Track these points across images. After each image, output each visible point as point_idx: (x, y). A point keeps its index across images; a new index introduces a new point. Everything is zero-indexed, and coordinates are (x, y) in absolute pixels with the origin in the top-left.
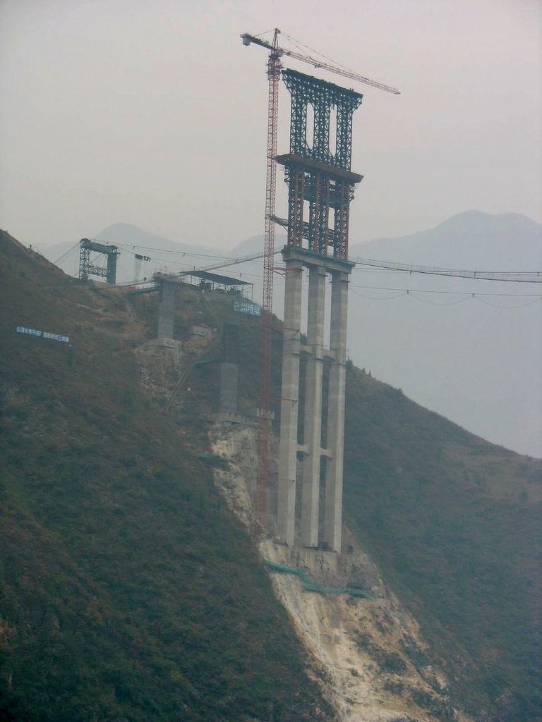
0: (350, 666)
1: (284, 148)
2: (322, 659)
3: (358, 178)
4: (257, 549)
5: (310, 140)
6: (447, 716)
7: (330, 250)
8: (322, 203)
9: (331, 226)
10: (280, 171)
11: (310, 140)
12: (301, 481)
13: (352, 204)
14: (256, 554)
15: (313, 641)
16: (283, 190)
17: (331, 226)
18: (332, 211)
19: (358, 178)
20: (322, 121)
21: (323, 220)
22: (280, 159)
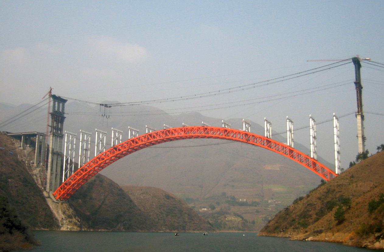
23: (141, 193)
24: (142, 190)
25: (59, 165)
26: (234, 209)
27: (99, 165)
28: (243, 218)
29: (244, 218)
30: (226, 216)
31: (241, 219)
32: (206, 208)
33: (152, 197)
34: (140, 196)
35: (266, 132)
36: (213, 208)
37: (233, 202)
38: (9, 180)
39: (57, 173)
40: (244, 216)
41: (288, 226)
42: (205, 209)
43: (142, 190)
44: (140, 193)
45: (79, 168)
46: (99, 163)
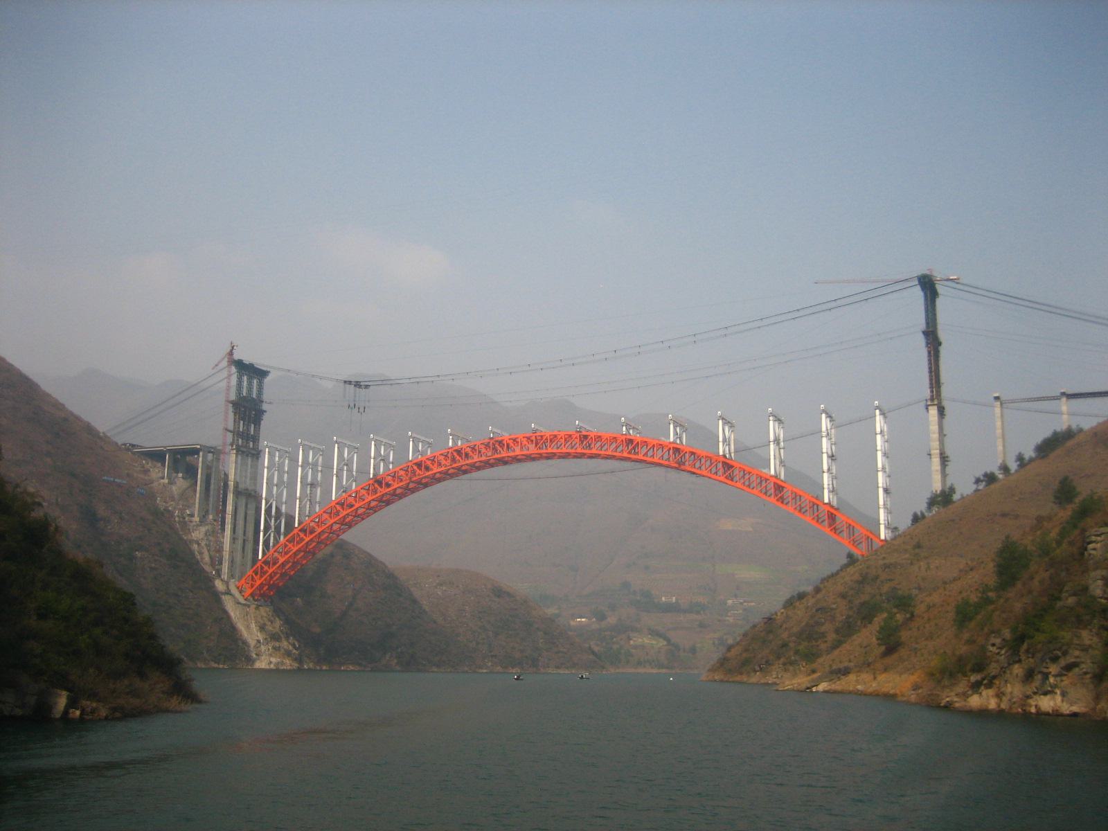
0: (257, 638)
1: (233, 397)
2: (217, 585)
3: (265, 411)
4: (214, 584)
5: (244, 393)
6: (492, 795)
7: (251, 445)
8: (247, 440)
9: (252, 433)
10: (231, 409)
11: (244, 393)
12: (231, 552)
13: (262, 422)
14: (214, 586)
15: (241, 626)
16: (231, 415)
17: (252, 433)
18: (253, 426)
19: (265, 411)
20: (250, 384)
21: (248, 430)
22: (232, 402)
24: (439, 576)
28: (668, 641)
31: (665, 643)
34: (436, 590)
36: (602, 617)
42: (583, 620)
44: (435, 584)
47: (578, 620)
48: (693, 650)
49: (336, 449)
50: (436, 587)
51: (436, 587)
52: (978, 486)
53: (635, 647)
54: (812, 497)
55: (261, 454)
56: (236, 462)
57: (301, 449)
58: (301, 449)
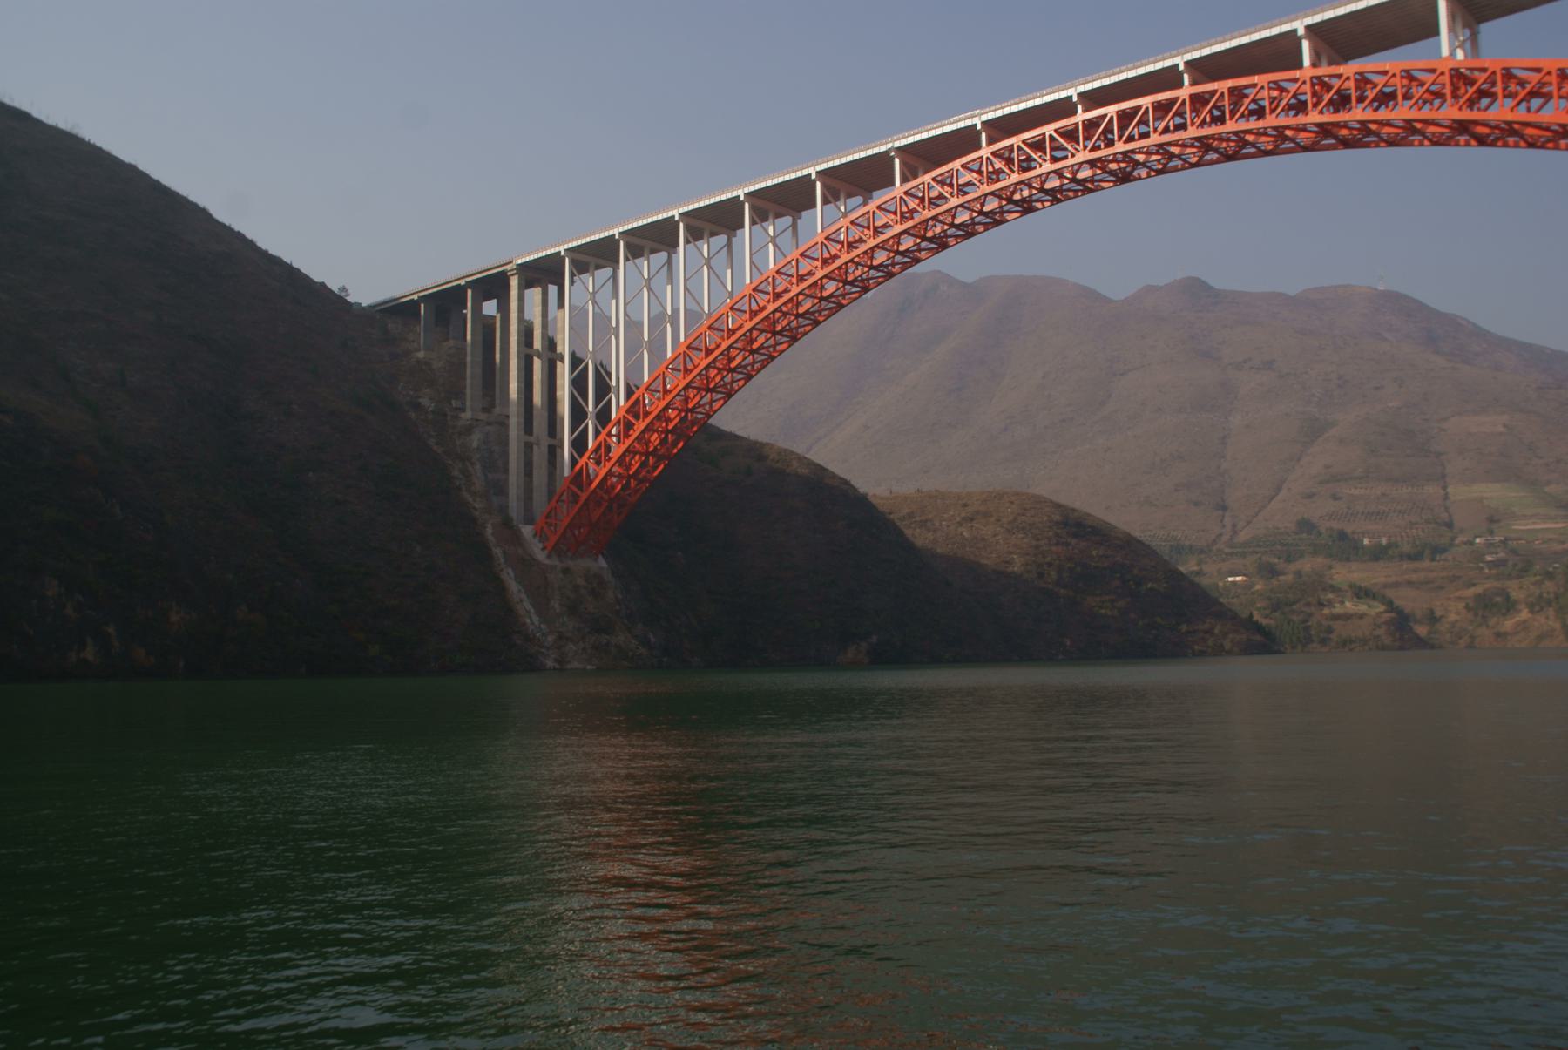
11: (509, 274)
23: (964, 519)
24: (965, 505)
25: (540, 455)
26: (1344, 574)
27: (1076, 167)
28: (1389, 604)
29: (1397, 603)
30: (1322, 597)
31: (1382, 608)
32: (1244, 575)
33: (1009, 531)
34: (960, 529)
35: (1230, 83)
36: (1271, 572)
37: (1345, 546)
38: (311, 474)
39: (532, 439)
40: (1390, 593)
41: (993, 519)
42: (1239, 579)
43: (965, 505)
44: (958, 519)
45: (819, 230)
46: (917, 218)
47: (1231, 579)
48: (1433, 619)
49: (469, 337)
50: (960, 524)
51: (960, 524)
52: (1305, 38)
53: (1336, 617)
54: (979, 187)
55: (558, 450)
56: (457, 993)
57: (33, 1043)
58: (33, 1043)
